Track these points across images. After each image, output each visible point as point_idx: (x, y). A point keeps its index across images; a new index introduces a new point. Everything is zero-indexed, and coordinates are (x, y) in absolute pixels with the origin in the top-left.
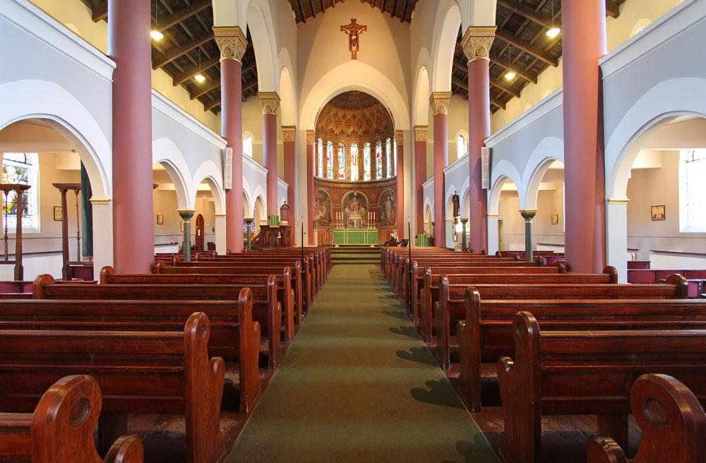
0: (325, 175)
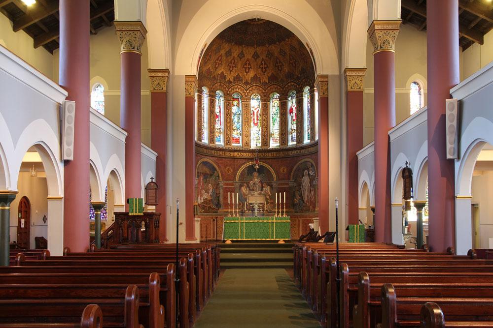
0: (212, 139)
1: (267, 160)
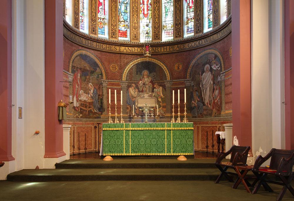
0: (93, 29)
1: (159, 56)
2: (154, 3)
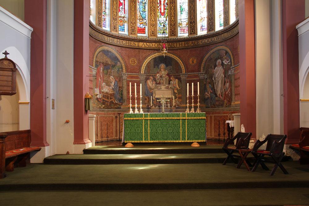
0: (114, 27)
2: (170, 3)
